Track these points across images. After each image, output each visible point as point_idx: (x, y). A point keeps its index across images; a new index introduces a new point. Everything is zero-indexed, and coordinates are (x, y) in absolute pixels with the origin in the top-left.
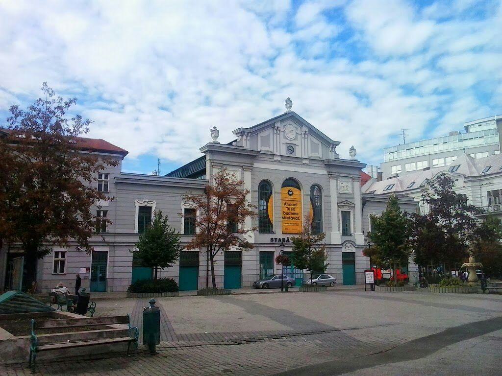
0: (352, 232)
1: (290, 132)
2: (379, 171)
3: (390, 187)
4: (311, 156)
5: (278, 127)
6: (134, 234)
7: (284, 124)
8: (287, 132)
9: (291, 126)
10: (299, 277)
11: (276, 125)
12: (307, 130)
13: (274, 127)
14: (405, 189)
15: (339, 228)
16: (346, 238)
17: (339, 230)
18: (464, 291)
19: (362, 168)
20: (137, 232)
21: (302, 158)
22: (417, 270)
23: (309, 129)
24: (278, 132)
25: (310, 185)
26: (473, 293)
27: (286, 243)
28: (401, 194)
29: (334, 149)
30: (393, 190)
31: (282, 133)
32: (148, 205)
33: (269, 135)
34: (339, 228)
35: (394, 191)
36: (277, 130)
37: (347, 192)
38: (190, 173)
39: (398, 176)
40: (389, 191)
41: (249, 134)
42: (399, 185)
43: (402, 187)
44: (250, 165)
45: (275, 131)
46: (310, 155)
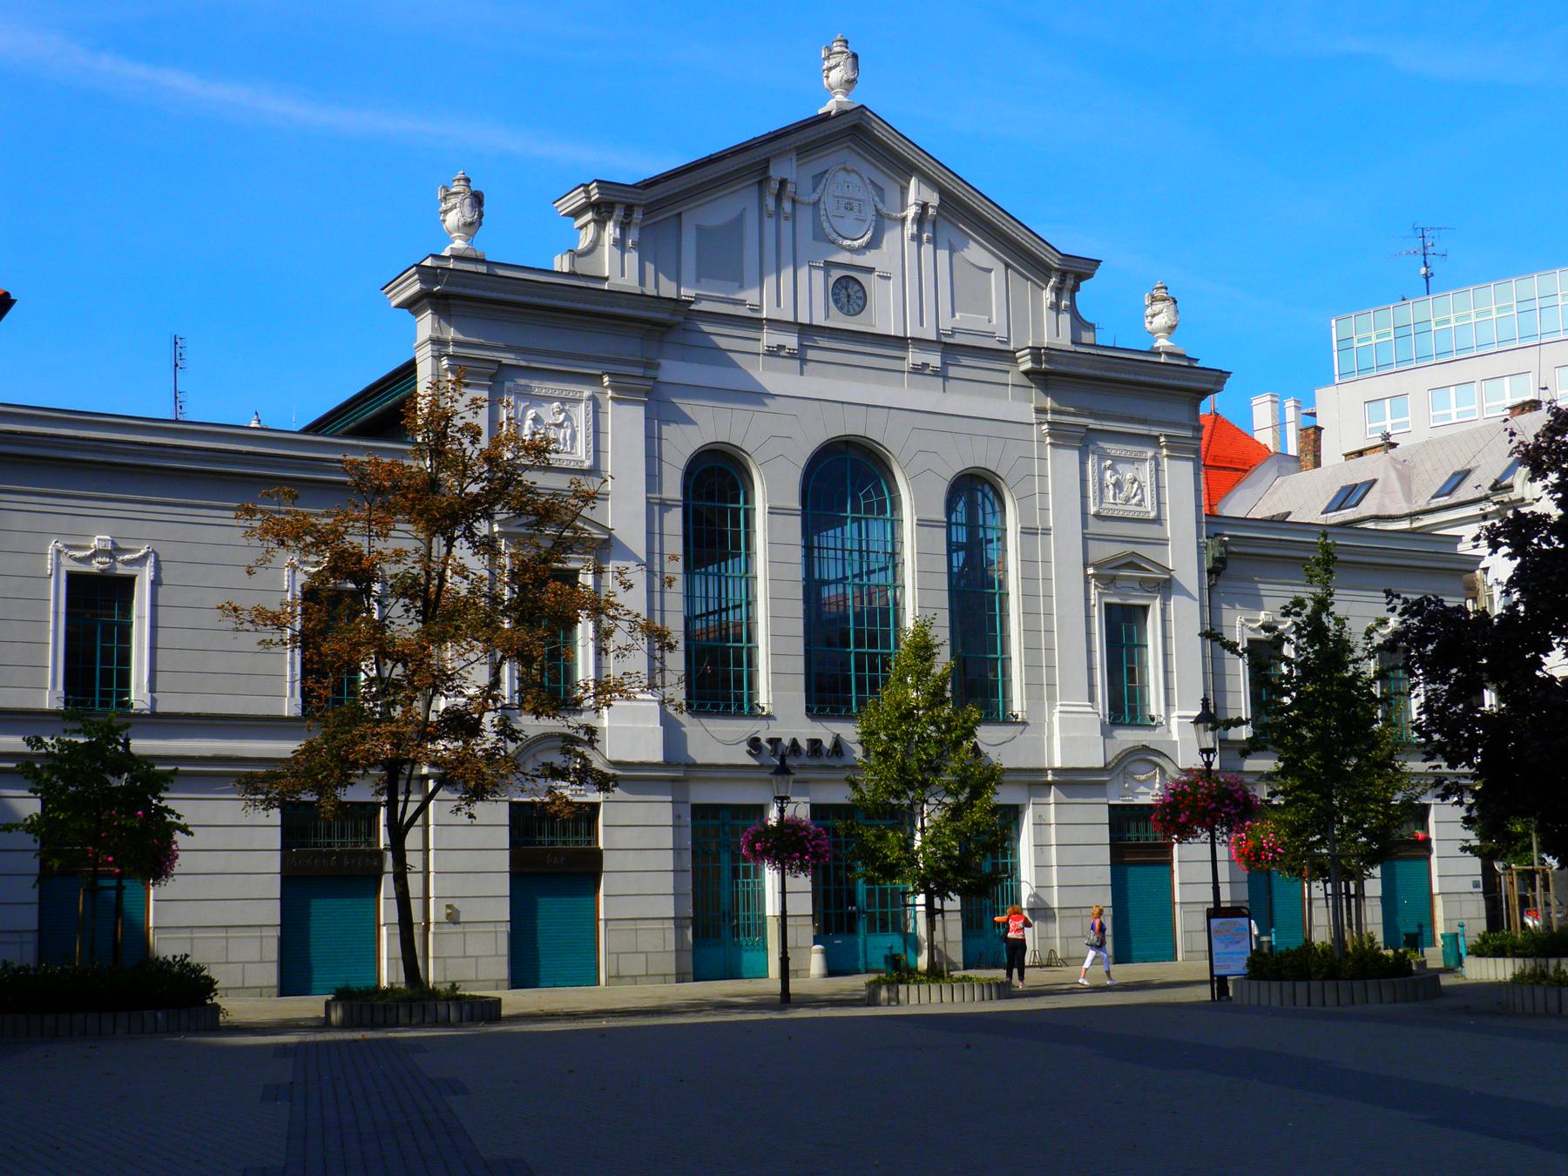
1: (849, 207)
2: (1310, 422)
3: (1349, 495)
4: (954, 332)
5: (783, 183)
6: (281, 719)
7: (817, 166)
8: (829, 203)
9: (854, 177)
10: (1254, 1001)
11: (777, 171)
12: (933, 199)
13: (763, 183)
14: (1421, 504)
15: (1091, 686)
16: (1128, 738)
17: (1092, 698)
19: (1204, 394)
20: (297, 711)
21: (901, 342)
23: (944, 193)
24: (787, 206)
25: (950, 474)
26: (1271, 899)
28: (1404, 525)
29: (1066, 295)
30: (1368, 507)
31: (805, 218)
33: (739, 220)
34: (1091, 686)
35: (1373, 512)
36: (779, 198)
37: (1131, 510)
38: (1335, 507)
39: (1394, 445)
40: (1348, 514)
42: (1397, 486)
43: (1408, 496)
45: (770, 203)
46: (946, 324)
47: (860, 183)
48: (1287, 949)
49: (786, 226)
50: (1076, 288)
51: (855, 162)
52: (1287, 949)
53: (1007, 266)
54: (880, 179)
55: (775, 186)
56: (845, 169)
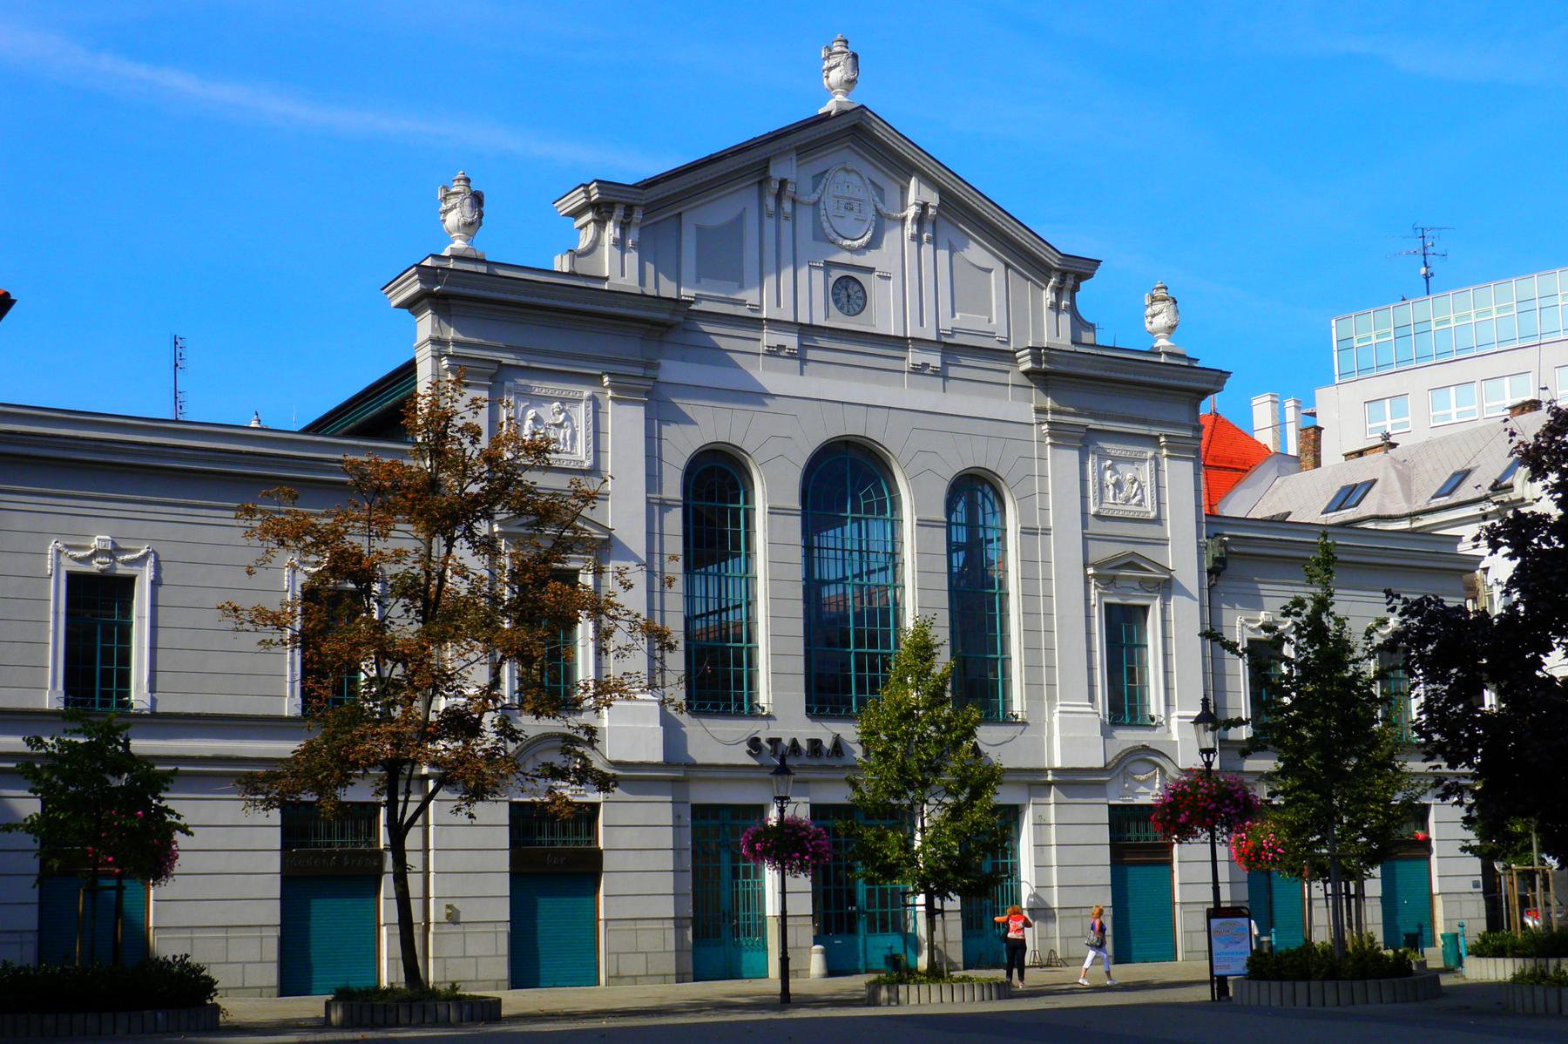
0: (1018, 706)
1: (849, 208)
3: (1349, 495)
4: (954, 332)
5: (783, 183)
6: (281, 719)
7: (817, 166)
8: (829, 203)
9: (854, 177)
11: (777, 171)
12: (933, 199)
14: (1421, 504)
15: (1091, 686)
16: (1128, 738)
17: (1092, 698)
18: (1429, 694)
19: (1204, 394)
20: (297, 712)
21: (901, 342)
22: (1476, 885)
23: (943, 192)
27: (804, 760)
28: (1404, 525)
30: (1368, 507)
31: (805, 218)
32: (121, 570)
33: (739, 221)
34: (1091, 686)
35: (1373, 513)
36: (779, 198)
37: (1131, 510)
41: (637, 216)
42: (1397, 485)
43: (1408, 497)
44: (639, 371)
45: (771, 203)
46: (946, 324)
47: (860, 183)
48: (1287, 949)
49: (786, 226)
50: (1076, 288)
51: (855, 162)
52: (1287, 949)
53: (1007, 266)
54: (880, 179)
55: (775, 186)
56: (845, 169)
